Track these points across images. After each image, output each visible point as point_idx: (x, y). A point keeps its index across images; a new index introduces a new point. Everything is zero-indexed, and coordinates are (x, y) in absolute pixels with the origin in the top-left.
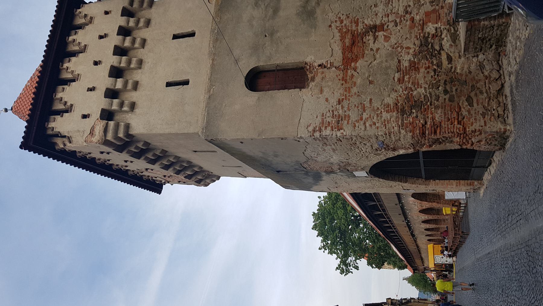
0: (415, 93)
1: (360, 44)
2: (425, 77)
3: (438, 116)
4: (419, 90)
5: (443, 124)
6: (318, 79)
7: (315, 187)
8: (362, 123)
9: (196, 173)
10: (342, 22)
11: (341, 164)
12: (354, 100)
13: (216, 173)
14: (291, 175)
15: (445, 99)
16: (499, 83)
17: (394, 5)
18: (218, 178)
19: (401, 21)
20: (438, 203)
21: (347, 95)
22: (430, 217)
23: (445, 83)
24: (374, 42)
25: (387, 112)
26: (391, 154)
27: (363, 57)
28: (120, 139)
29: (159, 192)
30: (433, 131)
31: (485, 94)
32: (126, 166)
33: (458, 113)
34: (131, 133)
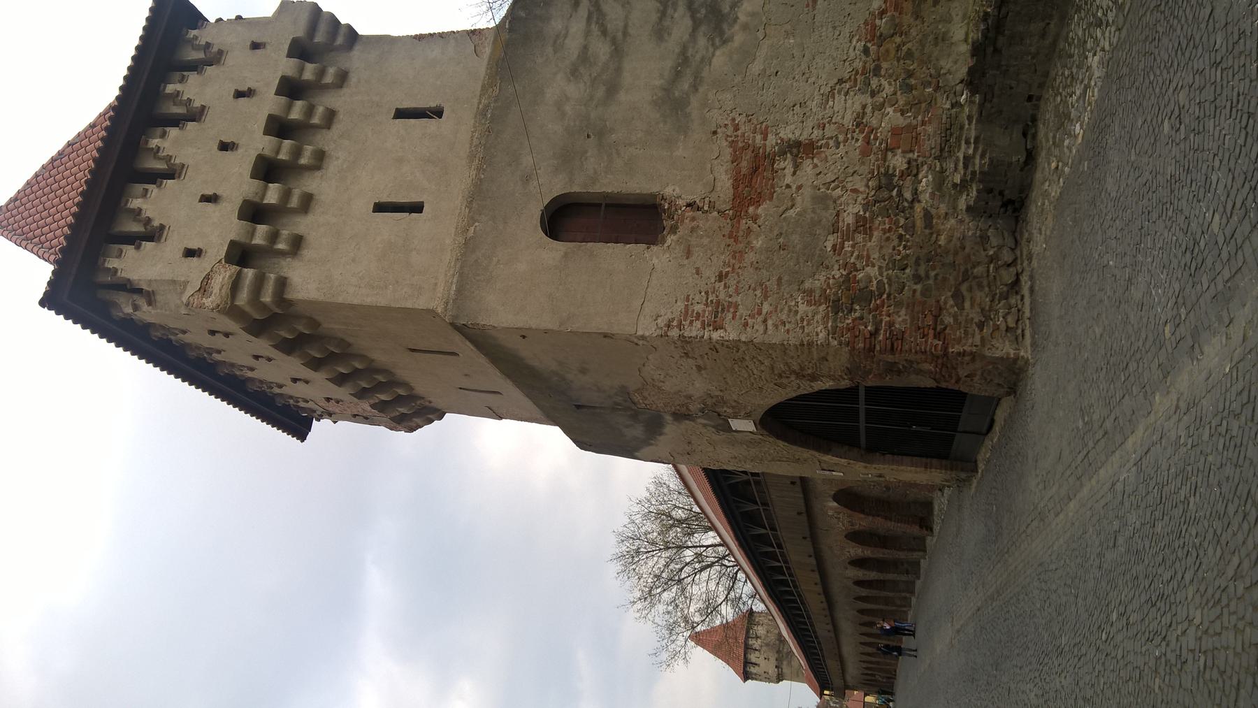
0: (860, 275)
1: (768, 174)
2: (881, 247)
3: (901, 319)
4: (868, 269)
5: (906, 336)
6: (682, 231)
7: (646, 450)
8: (760, 319)
9: (399, 400)
10: (736, 128)
11: (709, 402)
12: (749, 277)
13: (438, 403)
14: (602, 424)
15: (915, 291)
16: (1013, 270)
17: (836, 109)
18: (430, 414)
19: (846, 140)
20: (886, 518)
21: (737, 266)
22: (868, 552)
23: (917, 263)
24: (794, 173)
25: (809, 303)
26: (807, 388)
27: (771, 199)
28: (264, 306)
29: (302, 436)
30: (889, 347)
31: (987, 289)
32: (252, 369)
33: (936, 317)
34: (290, 295)
